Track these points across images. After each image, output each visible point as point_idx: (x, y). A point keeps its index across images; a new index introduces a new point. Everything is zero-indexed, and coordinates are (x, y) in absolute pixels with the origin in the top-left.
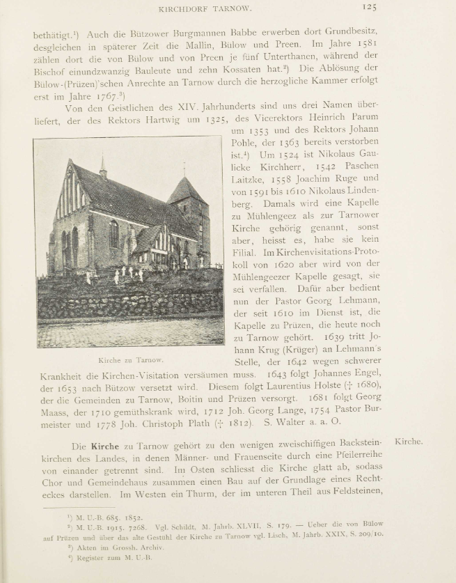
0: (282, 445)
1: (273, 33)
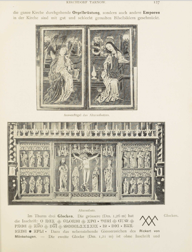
0: (59, 237)
1: (88, 13)
